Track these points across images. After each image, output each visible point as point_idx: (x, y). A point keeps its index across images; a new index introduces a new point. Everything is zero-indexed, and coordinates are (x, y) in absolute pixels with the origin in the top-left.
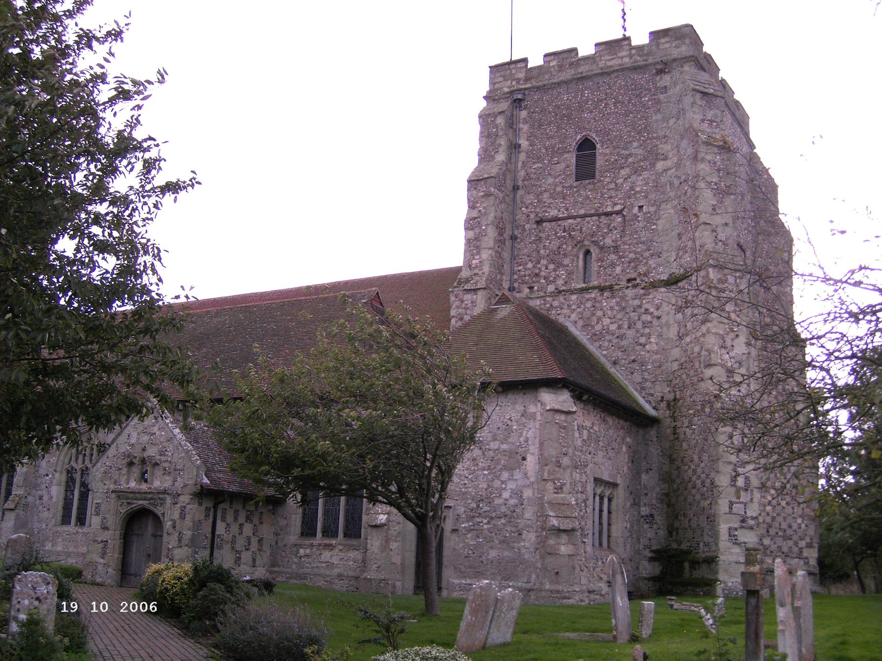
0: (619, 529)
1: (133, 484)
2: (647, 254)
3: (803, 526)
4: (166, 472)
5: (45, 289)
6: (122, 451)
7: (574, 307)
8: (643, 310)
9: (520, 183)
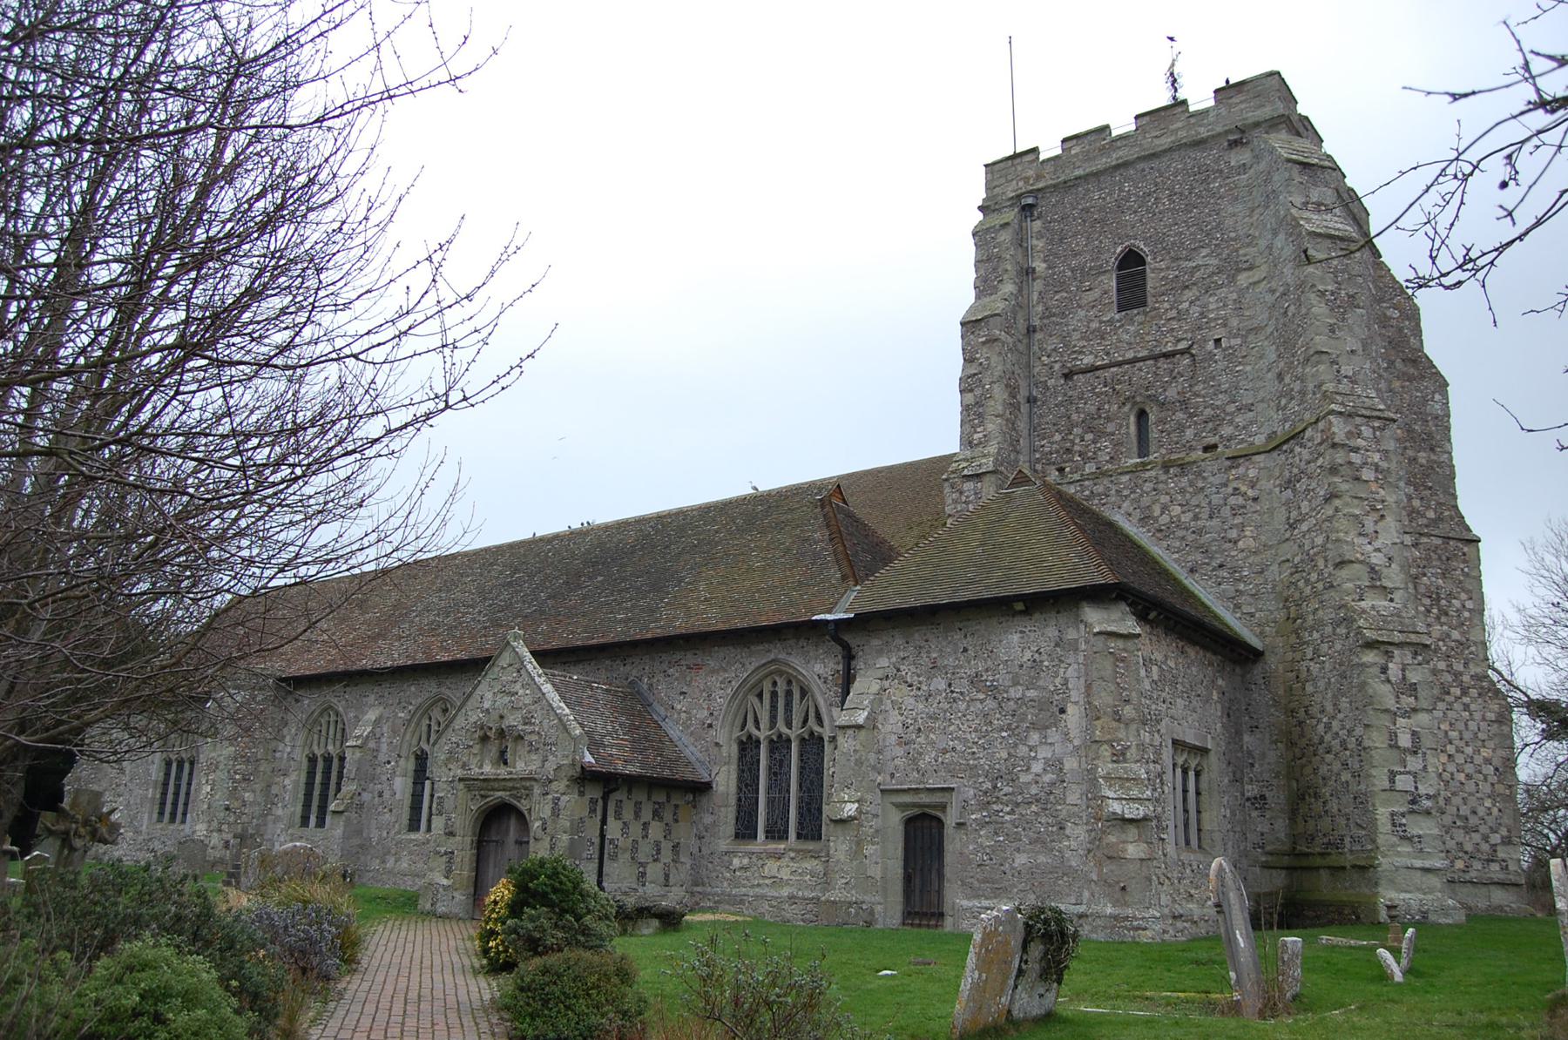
0: (1215, 817)
1: (488, 769)
2: (1231, 408)
3: (1495, 811)
4: (532, 749)
5: (69, 309)
6: (472, 720)
7: (1125, 493)
8: (1230, 490)
9: (1037, 322)
